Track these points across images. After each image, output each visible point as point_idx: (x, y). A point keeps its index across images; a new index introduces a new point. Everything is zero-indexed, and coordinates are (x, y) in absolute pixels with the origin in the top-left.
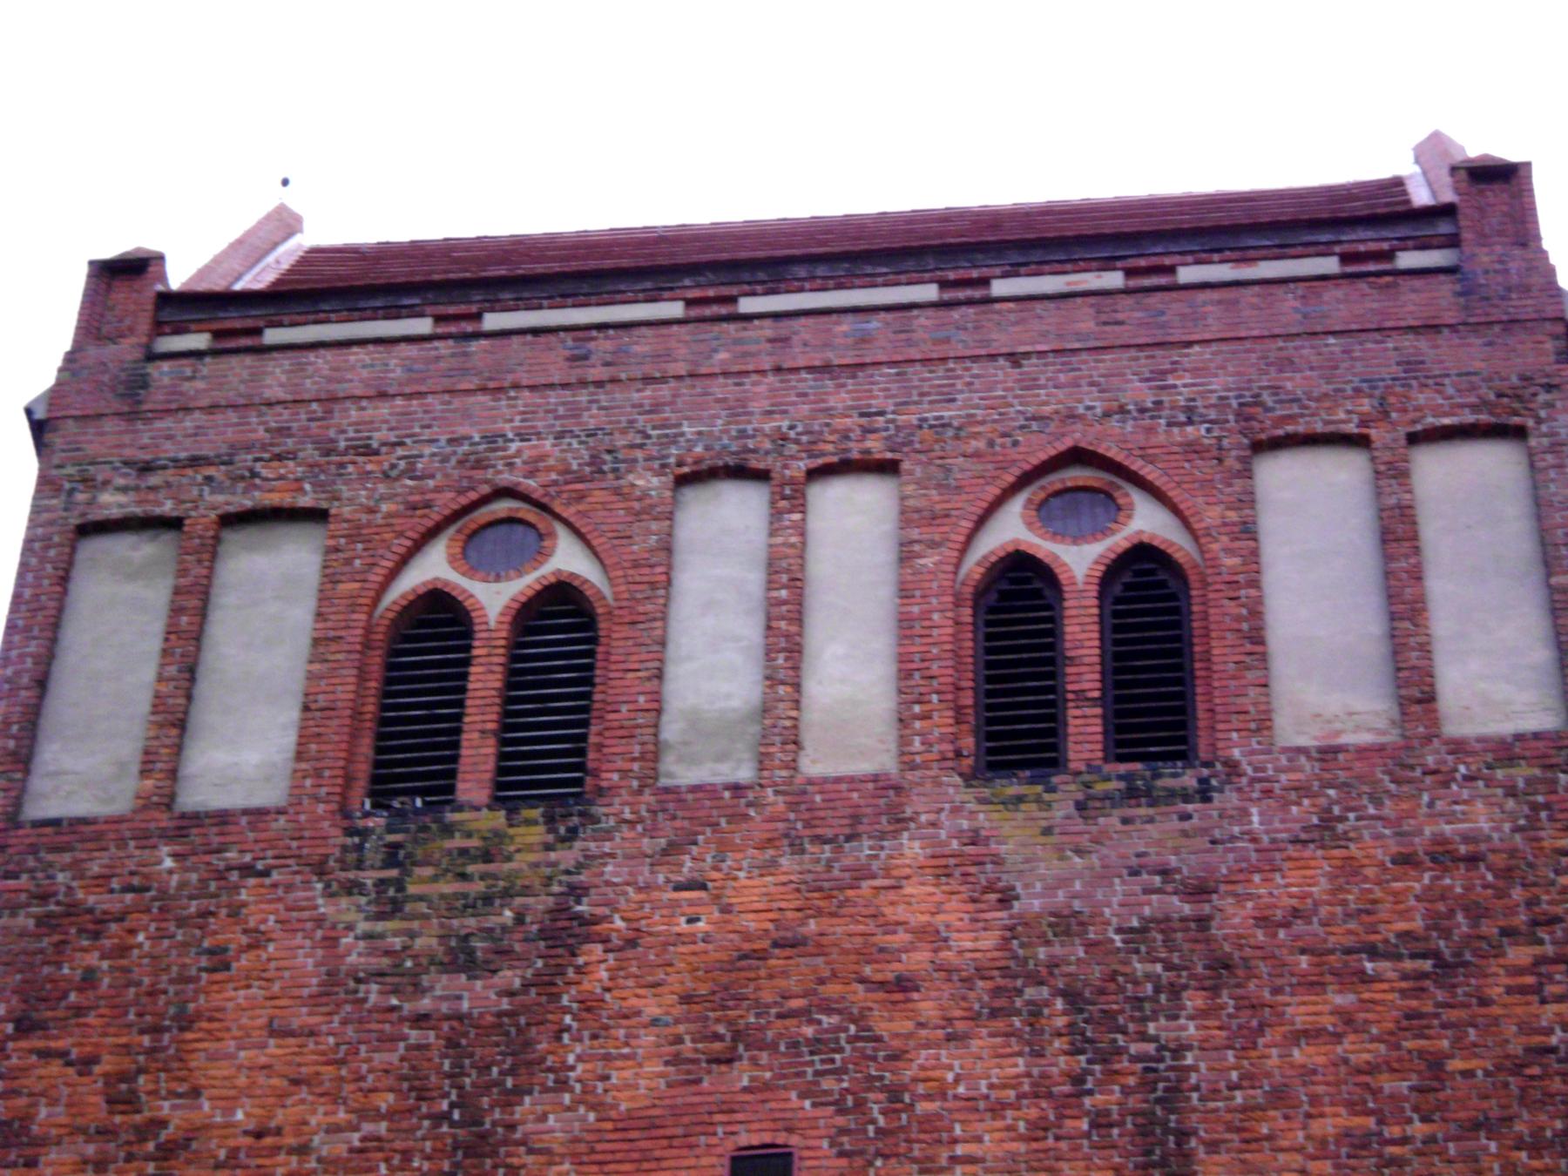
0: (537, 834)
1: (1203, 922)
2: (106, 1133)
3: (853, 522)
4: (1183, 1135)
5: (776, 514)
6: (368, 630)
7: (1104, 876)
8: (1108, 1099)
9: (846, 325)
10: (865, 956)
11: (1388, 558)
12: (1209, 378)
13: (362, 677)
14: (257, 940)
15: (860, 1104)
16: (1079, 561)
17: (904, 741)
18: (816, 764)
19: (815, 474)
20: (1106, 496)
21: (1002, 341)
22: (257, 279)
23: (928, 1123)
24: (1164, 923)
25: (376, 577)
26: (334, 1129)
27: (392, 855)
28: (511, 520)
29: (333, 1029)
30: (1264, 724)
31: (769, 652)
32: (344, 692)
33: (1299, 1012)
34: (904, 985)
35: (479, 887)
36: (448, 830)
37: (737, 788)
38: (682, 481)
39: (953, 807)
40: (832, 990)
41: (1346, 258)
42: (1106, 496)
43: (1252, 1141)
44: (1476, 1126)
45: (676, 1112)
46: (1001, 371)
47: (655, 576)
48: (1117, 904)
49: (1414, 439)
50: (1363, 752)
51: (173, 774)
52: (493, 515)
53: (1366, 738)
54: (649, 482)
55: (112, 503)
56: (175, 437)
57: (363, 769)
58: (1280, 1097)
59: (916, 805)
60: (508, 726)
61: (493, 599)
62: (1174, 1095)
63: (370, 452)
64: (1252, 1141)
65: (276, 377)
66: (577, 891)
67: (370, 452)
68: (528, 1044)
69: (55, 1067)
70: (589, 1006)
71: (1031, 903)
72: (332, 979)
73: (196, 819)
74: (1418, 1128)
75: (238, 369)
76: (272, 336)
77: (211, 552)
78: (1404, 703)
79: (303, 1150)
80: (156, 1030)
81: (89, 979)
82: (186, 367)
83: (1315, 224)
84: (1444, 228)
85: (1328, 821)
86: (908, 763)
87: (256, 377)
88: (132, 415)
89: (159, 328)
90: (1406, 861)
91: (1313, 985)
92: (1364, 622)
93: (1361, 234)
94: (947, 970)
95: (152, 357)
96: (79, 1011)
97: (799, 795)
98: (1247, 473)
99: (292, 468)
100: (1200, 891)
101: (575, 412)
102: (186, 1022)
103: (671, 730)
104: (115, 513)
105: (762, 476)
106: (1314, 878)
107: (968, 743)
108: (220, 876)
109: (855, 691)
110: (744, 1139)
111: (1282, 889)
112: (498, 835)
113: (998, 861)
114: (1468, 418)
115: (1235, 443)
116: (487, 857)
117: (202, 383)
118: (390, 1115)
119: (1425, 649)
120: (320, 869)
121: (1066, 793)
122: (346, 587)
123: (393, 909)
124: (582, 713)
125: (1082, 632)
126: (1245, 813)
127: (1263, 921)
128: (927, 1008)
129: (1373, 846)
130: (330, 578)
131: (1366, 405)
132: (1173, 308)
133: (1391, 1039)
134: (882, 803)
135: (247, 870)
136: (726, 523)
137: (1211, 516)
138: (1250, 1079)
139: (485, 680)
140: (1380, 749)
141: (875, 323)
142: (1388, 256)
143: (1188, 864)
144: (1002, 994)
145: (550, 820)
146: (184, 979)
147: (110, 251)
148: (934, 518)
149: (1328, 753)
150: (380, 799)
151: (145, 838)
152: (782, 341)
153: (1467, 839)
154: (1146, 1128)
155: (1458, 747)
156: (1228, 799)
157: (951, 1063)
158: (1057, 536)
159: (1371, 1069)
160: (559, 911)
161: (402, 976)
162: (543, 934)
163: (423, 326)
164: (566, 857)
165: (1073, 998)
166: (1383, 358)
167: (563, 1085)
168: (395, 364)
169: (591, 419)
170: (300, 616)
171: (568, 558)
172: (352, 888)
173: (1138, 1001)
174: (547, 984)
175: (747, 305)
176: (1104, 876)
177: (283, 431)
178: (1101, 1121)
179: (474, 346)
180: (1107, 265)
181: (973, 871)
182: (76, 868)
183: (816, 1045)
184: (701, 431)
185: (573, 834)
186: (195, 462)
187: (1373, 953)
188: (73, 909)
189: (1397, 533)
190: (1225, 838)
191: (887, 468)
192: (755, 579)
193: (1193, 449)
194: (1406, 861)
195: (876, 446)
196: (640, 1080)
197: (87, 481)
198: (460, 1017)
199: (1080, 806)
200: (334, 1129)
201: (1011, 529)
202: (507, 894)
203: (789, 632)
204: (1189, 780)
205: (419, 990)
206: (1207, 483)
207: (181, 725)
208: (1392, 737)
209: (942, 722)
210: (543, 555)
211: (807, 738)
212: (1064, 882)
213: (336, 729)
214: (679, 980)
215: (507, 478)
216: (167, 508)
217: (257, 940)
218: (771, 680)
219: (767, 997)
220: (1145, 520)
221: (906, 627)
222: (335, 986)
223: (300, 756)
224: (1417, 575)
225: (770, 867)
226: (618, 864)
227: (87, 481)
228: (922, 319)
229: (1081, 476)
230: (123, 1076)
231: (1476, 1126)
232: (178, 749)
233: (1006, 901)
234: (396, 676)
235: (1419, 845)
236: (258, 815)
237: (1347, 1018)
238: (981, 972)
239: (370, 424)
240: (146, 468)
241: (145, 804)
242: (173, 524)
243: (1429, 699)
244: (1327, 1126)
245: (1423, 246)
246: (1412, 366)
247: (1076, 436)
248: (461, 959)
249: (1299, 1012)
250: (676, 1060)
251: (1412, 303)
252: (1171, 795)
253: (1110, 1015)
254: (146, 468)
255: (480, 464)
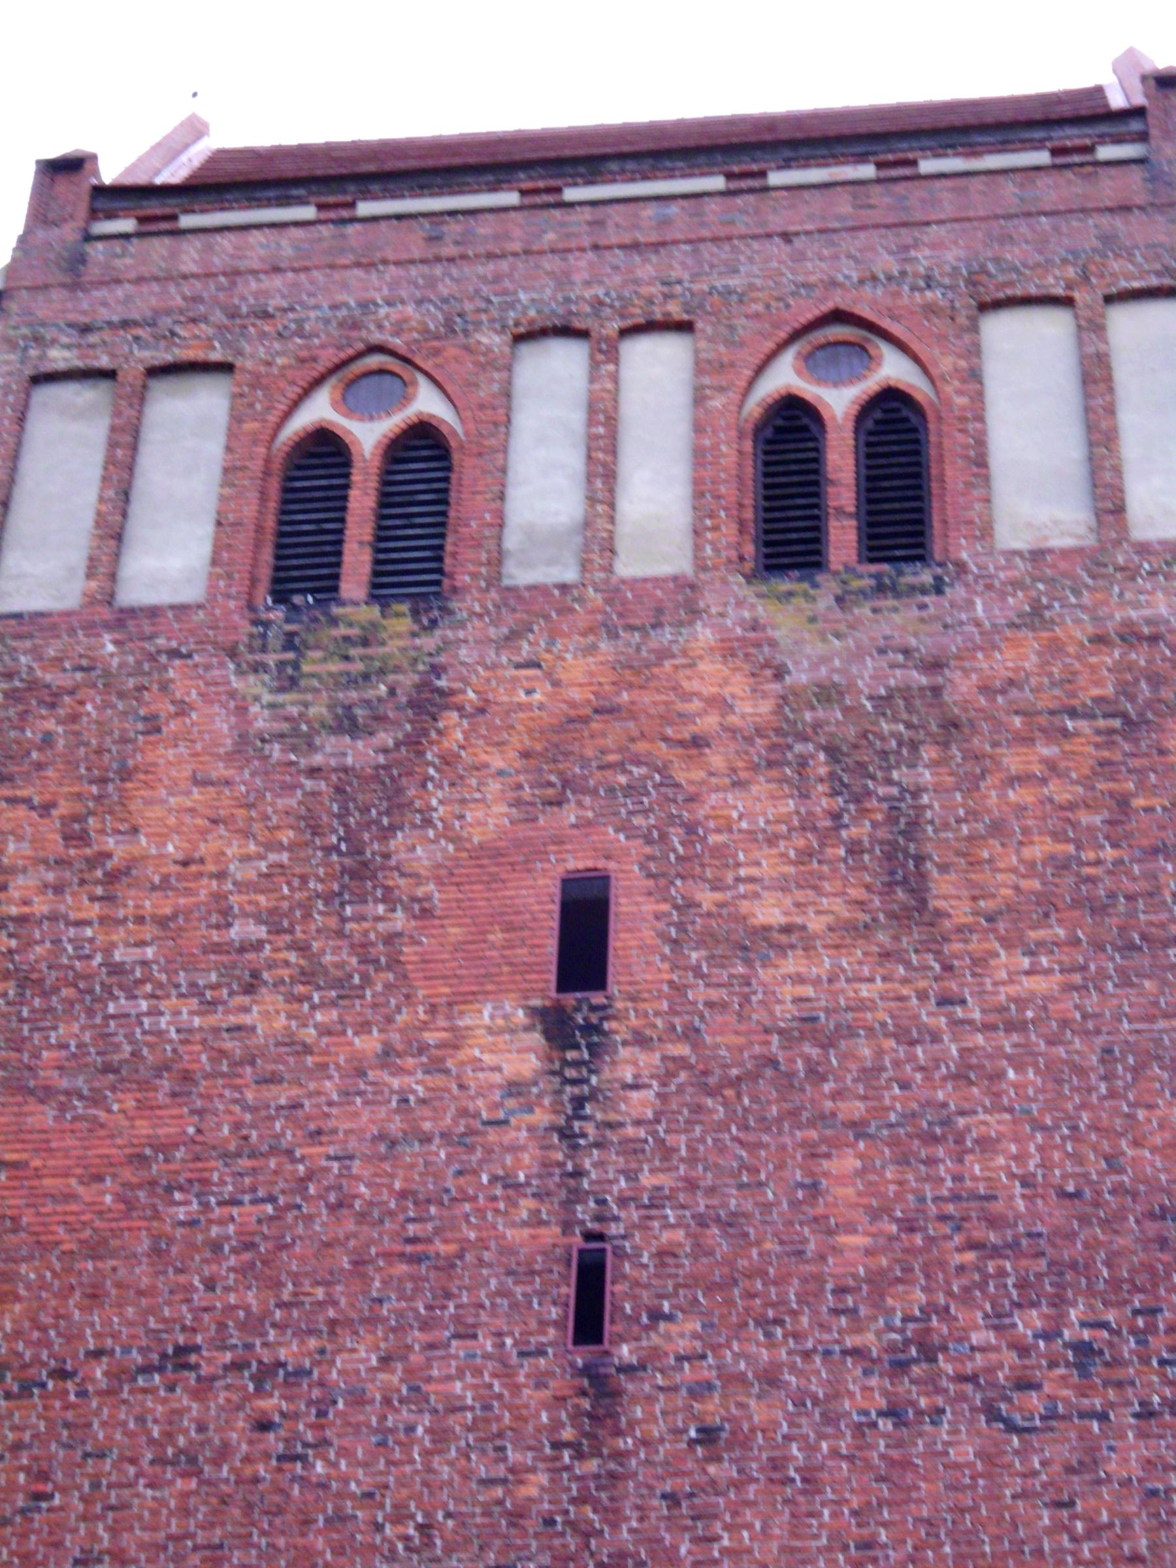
0: (405, 624)
1: (936, 690)
2: (62, 863)
3: (657, 371)
4: (919, 859)
5: (594, 365)
6: (268, 461)
7: (857, 655)
8: (861, 831)
9: (650, 212)
10: (666, 719)
11: (1087, 396)
12: (946, 252)
13: (263, 498)
14: (183, 709)
15: (664, 837)
16: (838, 402)
17: (698, 548)
18: (627, 567)
19: (629, 332)
20: (861, 348)
21: (776, 222)
22: (174, 174)
23: (718, 852)
24: (906, 692)
25: (273, 418)
26: (246, 859)
27: (290, 641)
28: (381, 372)
29: (244, 779)
30: (986, 532)
31: (590, 477)
32: (249, 511)
33: (1012, 761)
34: (698, 743)
35: (359, 667)
36: (334, 621)
37: (564, 588)
38: (519, 339)
39: (738, 601)
40: (641, 747)
41: (1055, 152)
42: (861, 348)
43: (975, 864)
44: (1154, 851)
45: (518, 844)
46: (777, 248)
47: (497, 415)
48: (869, 677)
49: (1109, 299)
50: (1066, 554)
51: (113, 577)
52: (368, 366)
53: (1068, 542)
54: (492, 340)
55: (60, 357)
56: (107, 304)
57: (265, 573)
58: (998, 828)
59: (709, 600)
60: (382, 537)
61: (368, 436)
62: (913, 828)
63: (266, 315)
64: (975, 864)
65: (190, 256)
66: (437, 670)
67: (266, 315)
68: (400, 791)
69: (21, 811)
70: (448, 760)
71: (800, 677)
72: (243, 739)
73: (132, 612)
74: (1109, 853)
75: (159, 247)
76: (186, 221)
77: (140, 398)
78: (1099, 514)
79: (221, 875)
80: (103, 781)
81: (48, 740)
82: (117, 247)
83: (1030, 124)
84: (1135, 126)
85: (1037, 609)
86: (701, 565)
87: (174, 255)
88: (75, 286)
89: (94, 214)
90: (1100, 640)
91: (1025, 740)
92: (1067, 447)
93: (1069, 131)
94: (732, 731)
95: (88, 238)
96: (39, 766)
97: (613, 592)
98: (974, 328)
99: (204, 329)
100: (934, 666)
101: (432, 283)
102: (126, 774)
103: (511, 541)
104: (61, 366)
105: (582, 334)
106: (1023, 656)
107: (749, 549)
108: (152, 658)
109: (661, 510)
110: (572, 864)
111: (1000, 663)
112: (374, 625)
113: (773, 643)
114: (1154, 281)
115: (964, 304)
116: (365, 642)
117: (128, 260)
118: (290, 848)
119: (1117, 470)
120: (233, 653)
121: (828, 586)
122: (249, 426)
123: (292, 684)
124: (440, 526)
125: (841, 460)
126: (970, 604)
127: (985, 689)
128: (716, 759)
129: (1075, 629)
130: (236, 418)
131: (1071, 272)
132: (915, 193)
133: (1087, 782)
134: (682, 598)
135: (174, 654)
136: (551, 379)
137: (945, 364)
138: (973, 815)
139: (362, 501)
140: (1079, 551)
141: (673, 209)
142: (1089, 150)
143: (924, 644)
144: (776, 750)
145: (415, 613)
146: (124, 740)
147: (54, 152)
148: (721, 367)
149: (1037, 555)
150: (281, 597)
151: (90, 628)
152: (598, 224)
153: (1149, 622)
154: (891, 854)
155: (1143, 549)
156: (956, 592)
157: (736, 803)
158: (820, 381)
159: (1072, 806)
160: (424, 685)
161: (299, 737)
162: (411, 704)
163: (308, 212)
164: (428, 642)
165: (832, 751)
166: (1086, 233)
167: (428, 822)
168: (286, 246)
169: (445, 288)
170: (214, 449)
171: (427, 402)
172: (258, 668)
173: (884, 754)
174: (415, 743)
175: (571, 194)
176: (857, 655)
177: (196, 299)
178: (855, 849)
179: (350, 229)
180: (861, 158)
181: (753, 652)
182: (36, 653)
183: (630, 790)
184: (534, 299)
185: (434, 623)
186: (126, 324)
187: (1073, 713)
188: (33, 685)
189: (1095, 376)
190: (958, 622)
191: (684, 327)
192: (577, 418)
193: (930, 309)
194: (1100, 640)
195: (675, 310)
196: (489, 818)
197: (37, 339)
198: (345, 770)
199: (839, 600)
200: (246, 859)
201: (784, 376)
202: (382, 672)
203: (603, 464)
204: (926, 577)
205: (311, 747)
206: (942, 338)
207: (118, 537)
208: (1090, 541)
209: (729, 531)
210: (406, 399)
211: (621, 545)
212: (825, 660)
213: (243, 540)
214: (518, 740)
215: (377, 337)
216: (104, 362)
217: (183, 709)
218: (592, 500)
219: (589, 752)
220: (893, 369)
221: (700, 457)
222: (246, 746)
223: (214, 562)
224: (1111, 410)
225: (592, 649)
226: (469, 646)
227: (37, 339)
228: (712, 207)
229: (840, 331)
230: (76, 818)
231: (1154, 851)
232: (117, 556)
233: (779, 674)
234: (291, 497)
235: (1111, 627)
236: (181, 610)
237: (1051, 765)
238: (759, 732)
239: (266, 293)
240: (86, 329)
241: (91, 600)
242: (109, 375)
243: (1119, 510)
244: (1035, 852)
245: (1118, 140)
246: (1108, 239)
247: (838, 300)
248: (347, 723)
249: (1012, 761)
250: (518, 803)
251: (1108, 188)
252: (912, 589)
253: (861, 765)
254: (86, 329)
255: (356, 326)
